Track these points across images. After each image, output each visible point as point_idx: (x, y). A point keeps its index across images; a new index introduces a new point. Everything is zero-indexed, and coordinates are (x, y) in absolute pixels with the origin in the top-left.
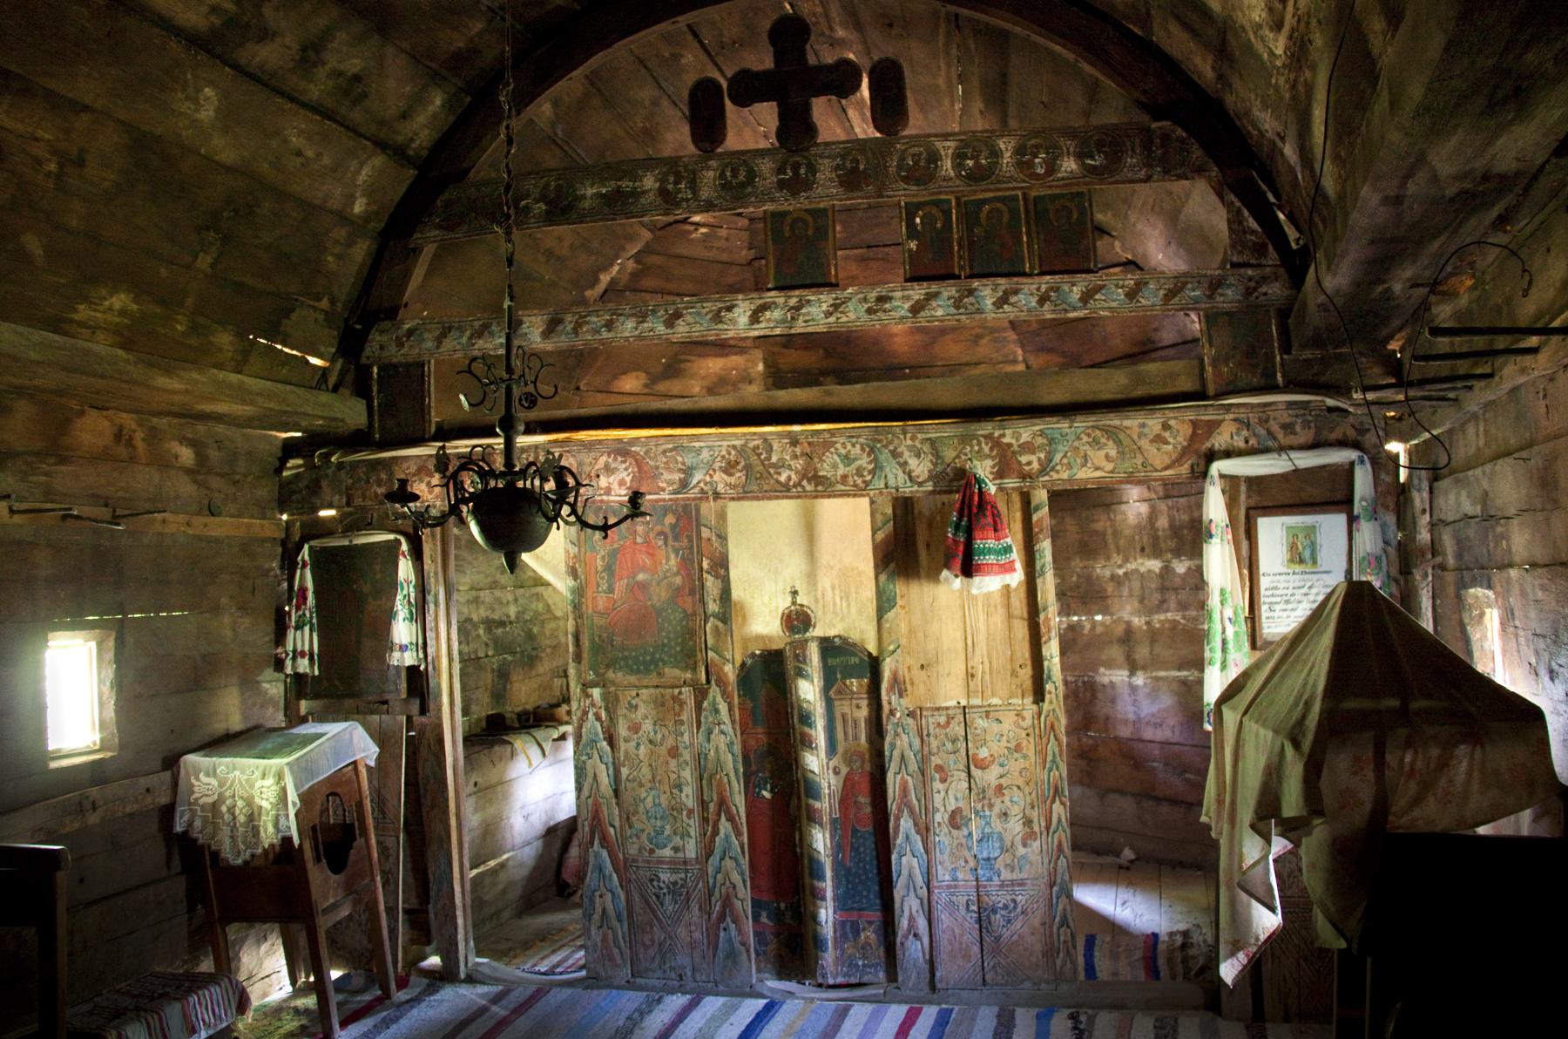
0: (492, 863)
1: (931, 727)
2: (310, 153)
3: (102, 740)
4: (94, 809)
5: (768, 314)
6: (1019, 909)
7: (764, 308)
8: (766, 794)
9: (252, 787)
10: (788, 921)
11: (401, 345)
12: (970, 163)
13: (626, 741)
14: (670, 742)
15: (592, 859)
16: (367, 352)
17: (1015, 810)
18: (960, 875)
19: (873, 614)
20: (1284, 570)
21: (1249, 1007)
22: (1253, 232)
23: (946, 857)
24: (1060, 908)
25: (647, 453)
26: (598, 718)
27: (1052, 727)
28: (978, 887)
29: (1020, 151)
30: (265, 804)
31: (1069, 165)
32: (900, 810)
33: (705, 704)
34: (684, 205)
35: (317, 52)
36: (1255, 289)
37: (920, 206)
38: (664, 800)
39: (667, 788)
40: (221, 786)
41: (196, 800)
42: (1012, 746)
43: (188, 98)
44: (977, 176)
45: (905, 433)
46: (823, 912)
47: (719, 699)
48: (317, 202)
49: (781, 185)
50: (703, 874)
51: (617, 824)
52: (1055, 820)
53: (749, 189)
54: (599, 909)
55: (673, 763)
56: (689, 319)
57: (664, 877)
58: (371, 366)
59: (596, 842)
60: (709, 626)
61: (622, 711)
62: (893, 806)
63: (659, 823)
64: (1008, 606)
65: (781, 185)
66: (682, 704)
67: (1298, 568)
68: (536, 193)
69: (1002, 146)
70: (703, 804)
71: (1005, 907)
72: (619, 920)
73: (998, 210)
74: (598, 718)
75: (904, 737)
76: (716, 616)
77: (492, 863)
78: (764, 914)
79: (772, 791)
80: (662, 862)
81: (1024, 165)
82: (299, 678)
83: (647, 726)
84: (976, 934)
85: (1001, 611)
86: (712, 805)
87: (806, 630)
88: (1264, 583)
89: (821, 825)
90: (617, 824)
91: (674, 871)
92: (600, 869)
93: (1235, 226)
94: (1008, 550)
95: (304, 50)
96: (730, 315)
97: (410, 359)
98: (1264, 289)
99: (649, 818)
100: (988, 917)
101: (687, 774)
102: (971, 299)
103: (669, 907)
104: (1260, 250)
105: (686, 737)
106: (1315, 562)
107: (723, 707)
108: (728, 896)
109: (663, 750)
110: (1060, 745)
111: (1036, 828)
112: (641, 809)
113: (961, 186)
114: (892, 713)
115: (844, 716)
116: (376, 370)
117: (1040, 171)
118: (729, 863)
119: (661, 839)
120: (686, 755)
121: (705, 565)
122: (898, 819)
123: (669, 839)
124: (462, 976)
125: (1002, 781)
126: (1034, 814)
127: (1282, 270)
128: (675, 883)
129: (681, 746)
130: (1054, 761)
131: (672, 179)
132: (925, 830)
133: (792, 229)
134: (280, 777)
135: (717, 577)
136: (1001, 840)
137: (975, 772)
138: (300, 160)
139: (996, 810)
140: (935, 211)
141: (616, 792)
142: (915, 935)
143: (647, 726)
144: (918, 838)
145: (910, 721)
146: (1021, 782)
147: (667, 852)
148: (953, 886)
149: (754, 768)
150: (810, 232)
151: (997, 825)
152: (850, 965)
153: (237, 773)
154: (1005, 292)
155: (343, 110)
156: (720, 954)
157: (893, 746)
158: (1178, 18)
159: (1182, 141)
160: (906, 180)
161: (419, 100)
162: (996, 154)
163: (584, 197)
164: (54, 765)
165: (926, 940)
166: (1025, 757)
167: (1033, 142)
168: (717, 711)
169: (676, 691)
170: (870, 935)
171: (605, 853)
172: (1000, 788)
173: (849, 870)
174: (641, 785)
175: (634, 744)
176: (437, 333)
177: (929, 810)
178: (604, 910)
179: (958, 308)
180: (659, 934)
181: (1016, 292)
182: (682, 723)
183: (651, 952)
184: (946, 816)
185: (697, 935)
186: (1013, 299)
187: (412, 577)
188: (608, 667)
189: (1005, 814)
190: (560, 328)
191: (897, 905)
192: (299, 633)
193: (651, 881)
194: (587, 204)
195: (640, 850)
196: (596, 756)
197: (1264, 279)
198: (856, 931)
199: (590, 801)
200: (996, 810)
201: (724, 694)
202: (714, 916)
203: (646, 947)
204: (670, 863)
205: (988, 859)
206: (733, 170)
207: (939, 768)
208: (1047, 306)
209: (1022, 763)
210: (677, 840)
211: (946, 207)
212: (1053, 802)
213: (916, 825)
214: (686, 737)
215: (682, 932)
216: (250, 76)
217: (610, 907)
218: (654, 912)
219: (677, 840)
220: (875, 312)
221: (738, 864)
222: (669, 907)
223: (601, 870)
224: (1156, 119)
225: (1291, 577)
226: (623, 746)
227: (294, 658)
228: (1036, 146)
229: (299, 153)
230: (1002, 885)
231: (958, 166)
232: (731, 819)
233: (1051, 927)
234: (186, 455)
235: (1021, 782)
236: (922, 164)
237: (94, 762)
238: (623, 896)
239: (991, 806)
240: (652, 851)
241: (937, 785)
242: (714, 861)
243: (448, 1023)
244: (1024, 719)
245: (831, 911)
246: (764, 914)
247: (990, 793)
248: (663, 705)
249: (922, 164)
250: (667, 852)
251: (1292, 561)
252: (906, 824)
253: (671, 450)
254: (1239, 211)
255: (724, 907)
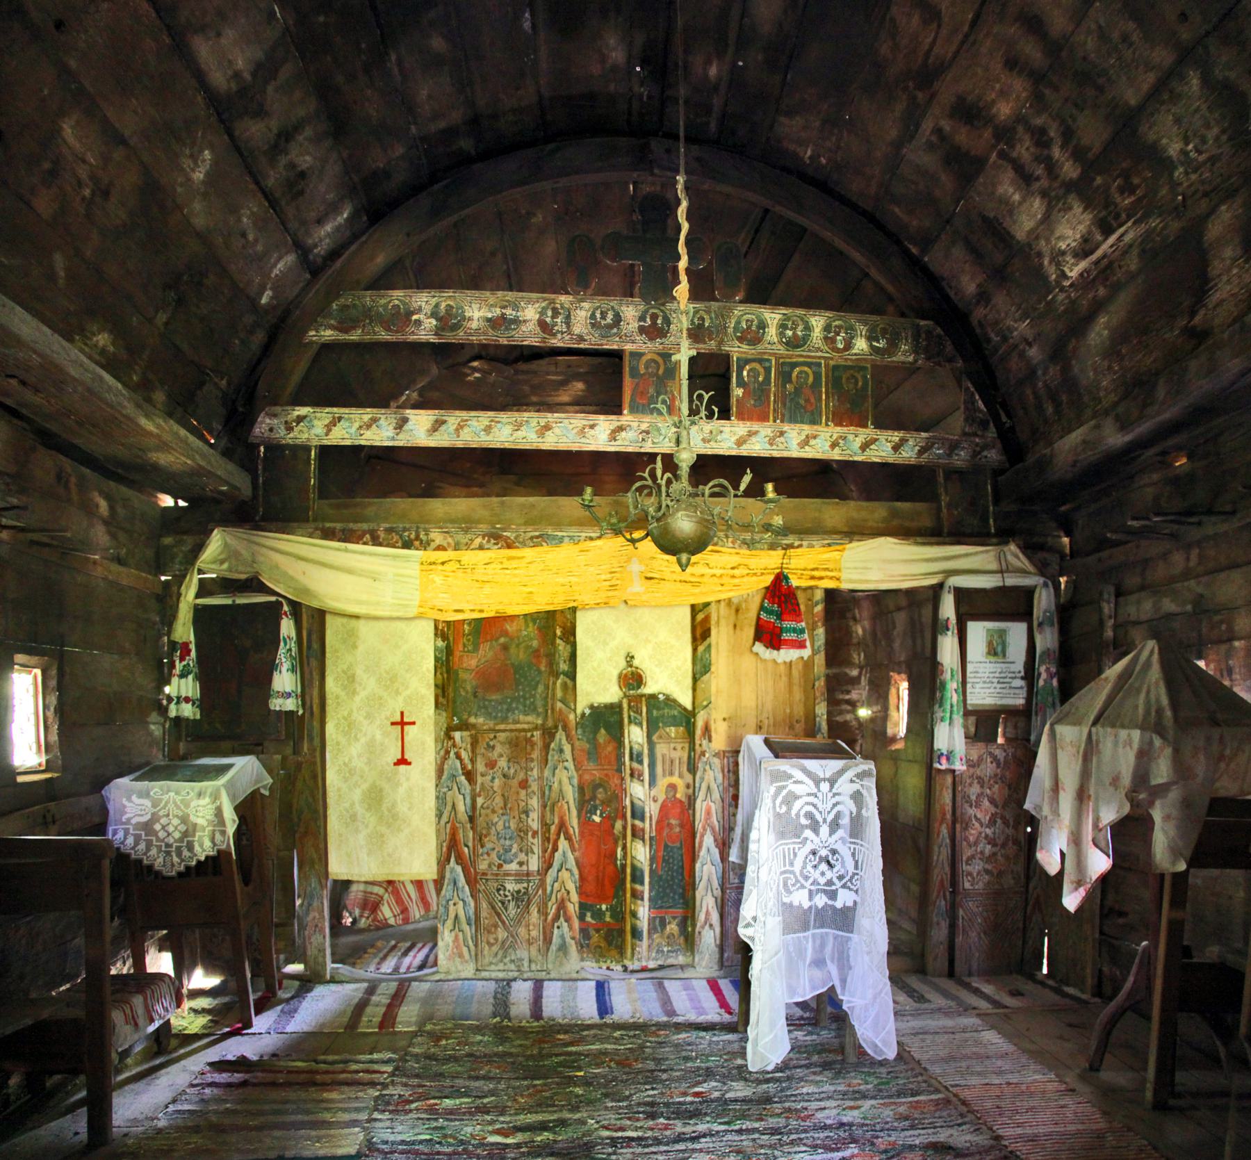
2: (251, 237)
3: (48, 761)
4: (54, 822)
5: (623, 434)
7: (620, 429)
8: (597, 819)
9: (187, 806)
10: (608, 919)
11: (290, 429)
12: (789, 333)
14: (521, 776)
15: (448, 875)
16: (257, 431)
19: (689, 681)
20: (983, 659)
21: (946, 969)
22: (981, 411)
25: (516, 538)
26: (458, 756)
29: (827, 328)
30: (201, 822)
31: (861, 345)
32: (705, 829)
33: (552, 745)
34: (559, 336)
35: (287, 141)
36: (979, 453)
37: (747, 361)
38: (513, 825)
40: (154, 806)
41: (129, 820)
43: (192, 156)
44: (794, 344)
45: (727, 537)
46: (641, 909)
47: (564, 741)
48: (241, 285)
49: (642, 330)
50: (542, 884)
51: (470, 844)
53: (615, 330)
54: (452, 915)
55: (523, 792)
56: (557, 431)
58: (259, 445)
59: (453, 859)
60: (559, 681)
61: (481, 749)
62: (699, 826)
63: (508, 842)
64: (790, 675)
65: (642, 330)
66: (533, 745)
67: (993, 659)
68: (427, 309)
69: (814, 323)
70: (545, 825)
72: (469, 924)
73: (806, 373)
74: (458, 756)
75: (711, 773)
76: (565, 674)
78: (589, 914)
81: (829, 341)
82: (178, 720)
83: (503, 763)
85: (784, 679)
86: (553, 828)
87: (639, 687)
88: (970, 668)
89: (643, 840)
90: (470, 844)
91: (518, 881)
93: (970, 406)
94: (802, 631)
95: (279, 135)
96: (592, 432)
97: (297, 442)
98: (985, 453)
99: (499, 839)
101: (534, 802)
102: (782, 439)
103: (512, 910)
104: (984, 425)
105: (535, 773)
106: (1004, 656)
107: (567, 748)
108: (563, 900)
109: (515, 783)
112: (493, 831)
113: (781, 350)
114: (703, 754)
115: (663, 756)
116: (262, 449)
117: (841, 346)
118: (565, 875)
119: (509, 856)
120: (534, 787)
121: (558, 632)
122: (702, 836)
123: (515, 855)
124: (328, 977)
127: (998, 441)
128: (518, 892)
129: (530, 779)
131: (550, 313)
133: (647, 368)
134: (215, 796)
135: (567, 642)
138: (243, 241)
140: (756, 365)
141: (472, 819)
142: (711, 926)
143: (503, 763)
147: (513, 867)
149: (587, 797)
150: (661, 372)
152: (658, 952)
153: (172, 794)
154: (807, 436)
155: (283, 203)
156: (554, 947)
157: (702, 779)
158: (967, 242)
159: (939, 336)
160: (740, 339)
161: (334, 209)
162: (808, 328)
163: (470, 319)
164: (20, 779)
165: (718, 929)
167: (837, 323)
168: (561, 751)
169: (529, 734)
170: (673, 927)
171: (459, 869)
173: (660, 877)
174: (494, 811)
175: (489, 778)
176: (327, 422)
178: (456, 917)
179: (771, 444)
181: (815, 437)
182: (532, 760)
183: (495, 948)
185: (534, 933)
186: (812, 442)
187: (293, 634)
190: (443, 428)
191: (698, 903)
192: (183, 680)
193: (498, 890)
194: (474, 325)
195: (490, 866)
196: (455, 788)
197: (985, 447)
198: (663, 924)
199: (449, 826)
201: (568, 737)
202: (550, 917)
204: (516, 875)
206: (602, 313)
208: (837, 450)
210: (522, 857)
211: (767, 364)
214: (535, 773)
215: (522, 931)
216: (238, 149)
218: (499, 915)
219: (522, 857)
220: (709, 441)
221: (572, 874)
222: (512, 910)
223: (455, 883)
224: (923, 318)
225: (988, 665)
226: (480, 780)
227: (178, 703)
228: (840, 327)
229: (244, 235)
231: (782, 334)
232: (568, 838)
234: (103, 505)
236: (754, 328)
237: (47, 780)
238: (472, 904)
240: (500, 866)
242: (552, 873)
243: (342, 1013)
245: (647, 909)
246: (589, 914)
248: (517, 745)
249: (754, 328)
250: (513, 867)
251: (989, 653)
253: (537, 537)
254: (973, 394)
255: (558, 910)
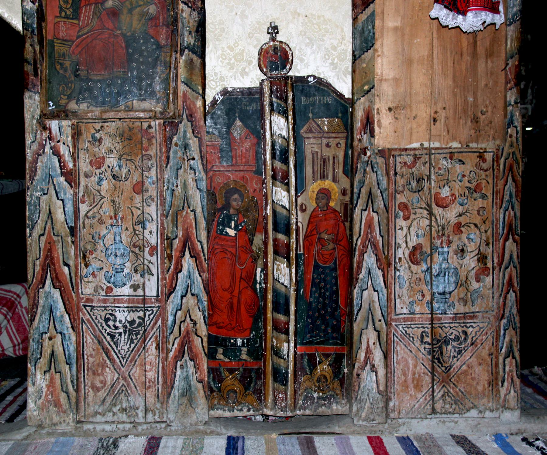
0: (270, 296)
1: (399, 166)
6: (469, 341)
10: (244, 357)
13: (87, 176)
14: (136, 177)
17: (471, 247)
18: (417, 309)
23: (405, 291)
24: (507, 339)
26: (56, 152)
27: (511, 169)
28: (432, 319)
32: (365, 246)
39: (130, 225)
42: (472, 186)
47: (189, 134)
51: (71, 263)
52: (507, 256)
54: (47, 352)
55: (138, 198)
57: (120, 316)
59: (48, 282)
71: (457, 338)
75: (374, 176)
77: (270, 296)
78: (220, 350)
79: (236, 228)
80: (119, 301)
83: (112, 161)
84: (428, 364)
91: (132, 309)
92: (510, 73)
99: (107, 256)
100: (441, 348)
109: (127, 186)
110: (516, 185)
111: (490, 265)
118: (190, 301)
120: (152, 191)
122: (362, 254)
125: (461, 219)
126: (489, 251)
128: (132, 322)
130: (510, 201)
132: (386, 264)
136: (457, 275)
137: (438, 211)
139: (454, 247)
143: (112, 161)
144: (380, 273)
145: (380, 160)
146: (478, 220)
148: (410, 320)
151: (454, 260)
156: (176, 392)
166: (484, 197)
168: (186, 147)
171: (56, 294)
172: (458, 227)
174: (101, 222)
175: (96, 179)
177: (389, 243)
178: (53, 354)
180: (110, 376)
182: (149, 158)
183: (102, 394)
184: (407, 252)
188: (70, 98)
189: (462, 251)
191: (356, 338)
193: (107, 320)
195: (96, 290)
198: (313, 363)
199: (43, 239)
200: (454, 247)
203: (96, 389)
205: (444, 293)
207: (404, 207)
209: (480, 203)
210: (137, 278)
212: (506, 239)
213: (378, 260)
217: (59, 349)
218: (107, 352)
226: (83, 182)
230: (455, 318)
233: (497, 358)
235: (478, 220)
238: (74, 338)
239: (449, 243)
240: (109, 290)
241: (401, 222)
244: (484, 160)
247: (449, 231)
252: (370, 260)
255: (182, 346)
